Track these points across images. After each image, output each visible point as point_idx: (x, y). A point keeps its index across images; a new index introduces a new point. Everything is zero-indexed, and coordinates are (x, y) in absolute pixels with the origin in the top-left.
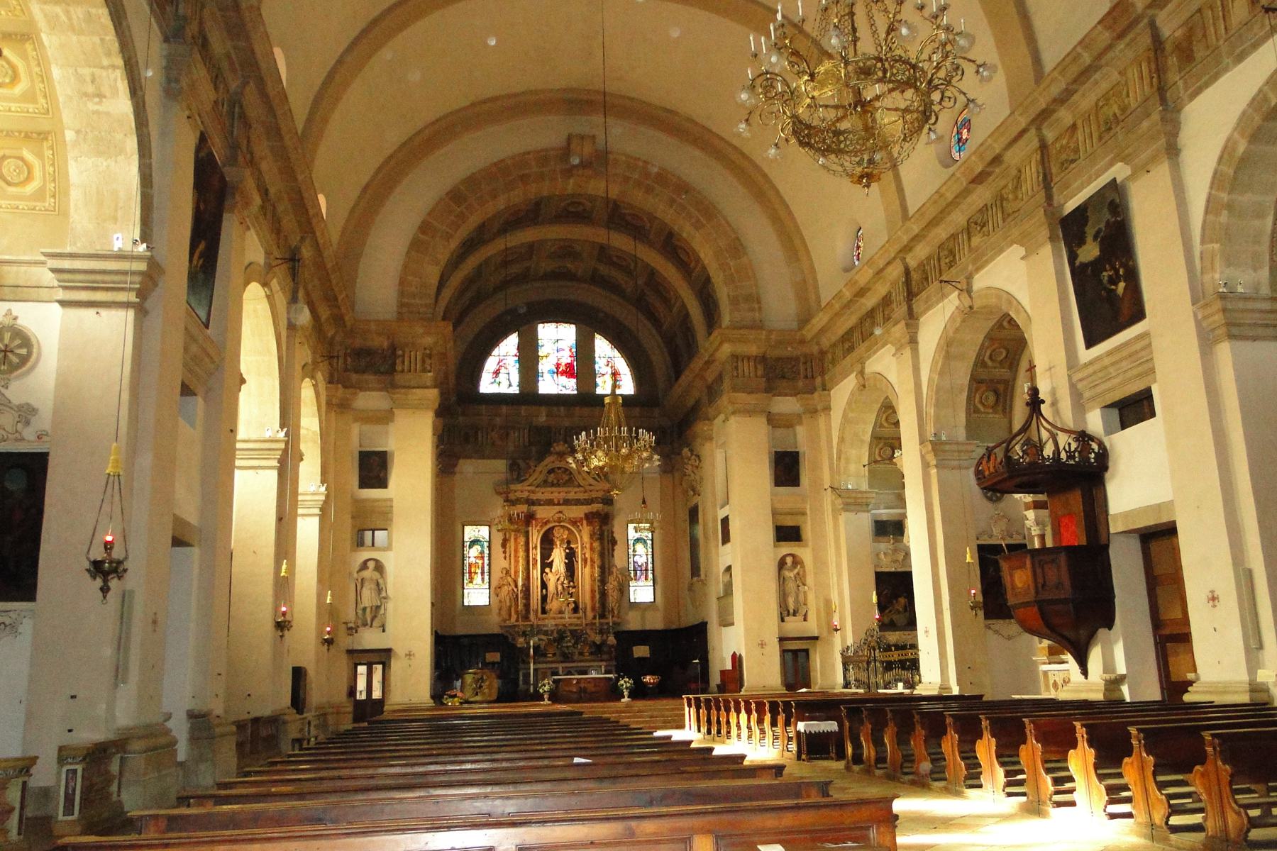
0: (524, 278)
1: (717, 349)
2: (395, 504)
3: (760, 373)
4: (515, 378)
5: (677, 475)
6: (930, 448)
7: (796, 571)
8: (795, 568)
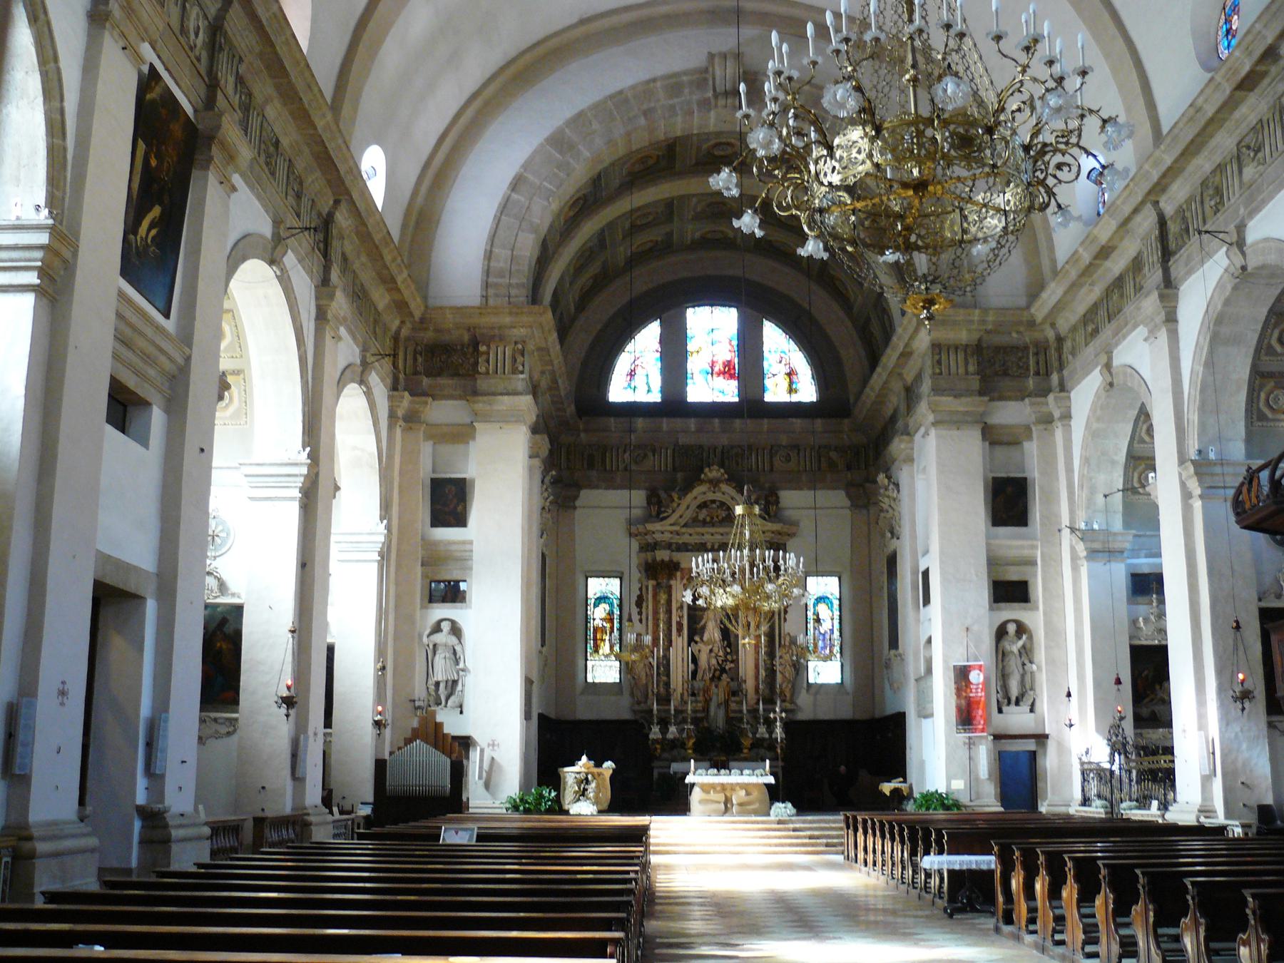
0: (665, 248)
1: (912, 338)
2: (475, 547)
3: (971, 368)
4: (656, 382)
5: (873, 510)
6: (1192, 469)
7: (1020, 643)
8: (1020, 638)
